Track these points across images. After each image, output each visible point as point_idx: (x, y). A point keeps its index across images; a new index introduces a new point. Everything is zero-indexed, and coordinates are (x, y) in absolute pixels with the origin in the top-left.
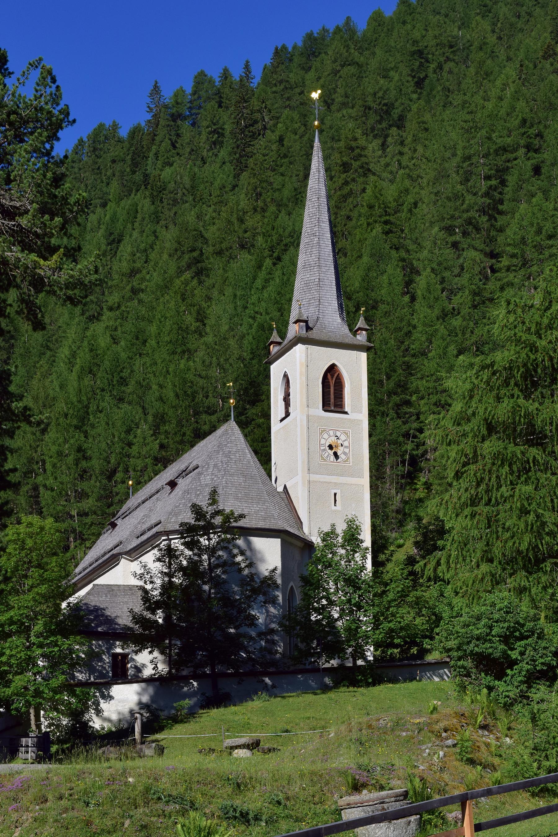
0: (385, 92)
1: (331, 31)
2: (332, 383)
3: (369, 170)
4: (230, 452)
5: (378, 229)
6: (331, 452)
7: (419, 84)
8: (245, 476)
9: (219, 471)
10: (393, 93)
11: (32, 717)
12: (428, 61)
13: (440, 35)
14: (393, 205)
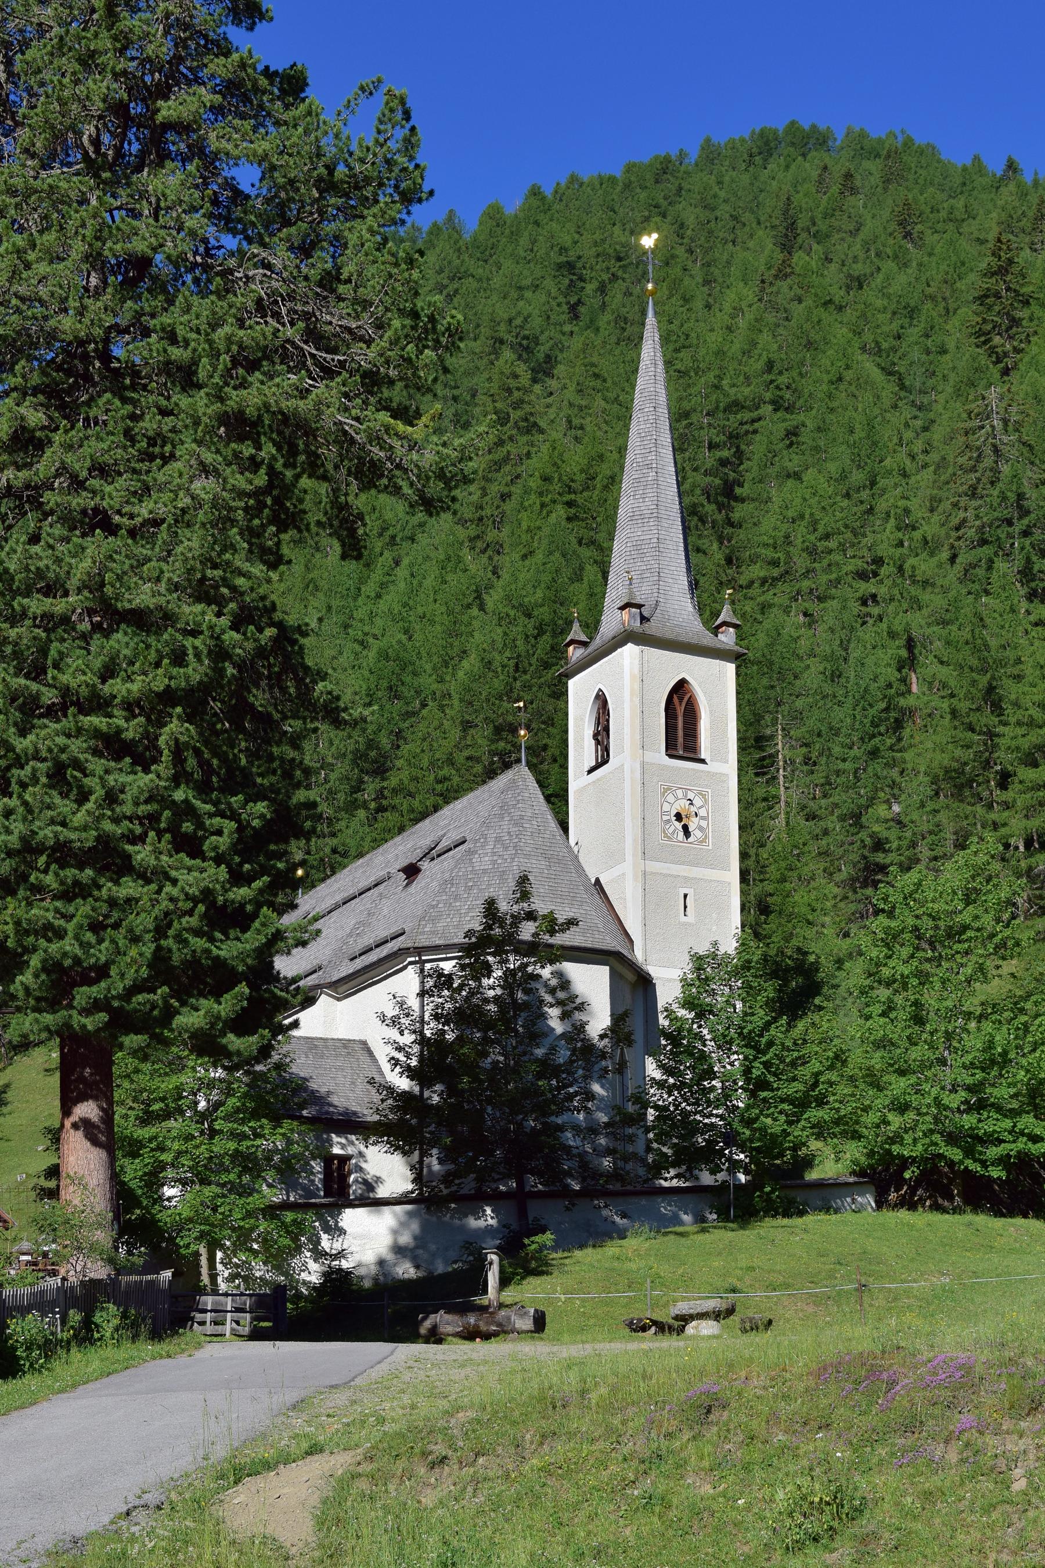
0: (526, 319)
1: (425, 229)
2: (680, 710)
3: (535, 424)
4: (522, 817)
5: (560, 512)
6: (679, 826)
7: (574, 310)
8: (548, 859)
9: (506, 848)
10: (537, 322)
11: (204, 1261)
12: (581, 279)
13: (603, 241)
14: (580, 477)
